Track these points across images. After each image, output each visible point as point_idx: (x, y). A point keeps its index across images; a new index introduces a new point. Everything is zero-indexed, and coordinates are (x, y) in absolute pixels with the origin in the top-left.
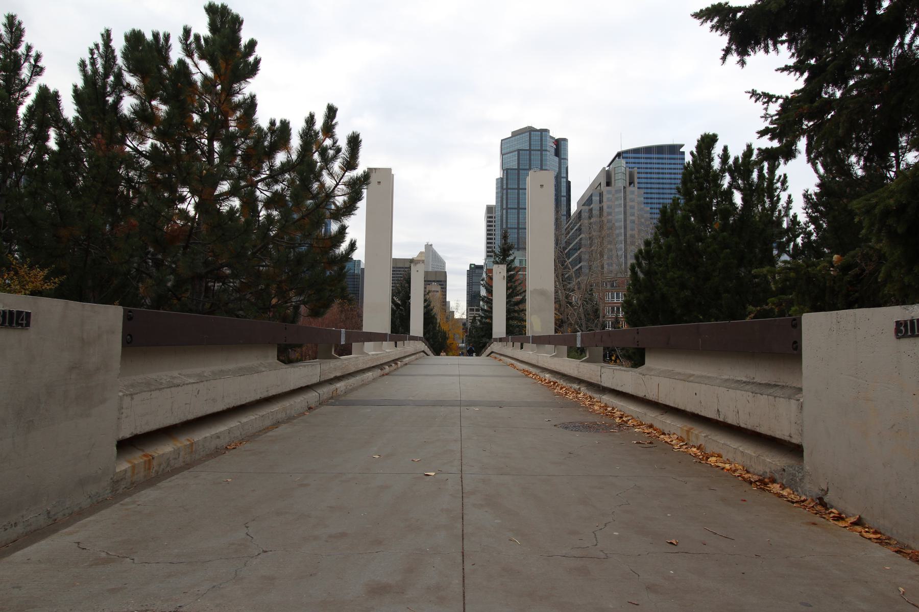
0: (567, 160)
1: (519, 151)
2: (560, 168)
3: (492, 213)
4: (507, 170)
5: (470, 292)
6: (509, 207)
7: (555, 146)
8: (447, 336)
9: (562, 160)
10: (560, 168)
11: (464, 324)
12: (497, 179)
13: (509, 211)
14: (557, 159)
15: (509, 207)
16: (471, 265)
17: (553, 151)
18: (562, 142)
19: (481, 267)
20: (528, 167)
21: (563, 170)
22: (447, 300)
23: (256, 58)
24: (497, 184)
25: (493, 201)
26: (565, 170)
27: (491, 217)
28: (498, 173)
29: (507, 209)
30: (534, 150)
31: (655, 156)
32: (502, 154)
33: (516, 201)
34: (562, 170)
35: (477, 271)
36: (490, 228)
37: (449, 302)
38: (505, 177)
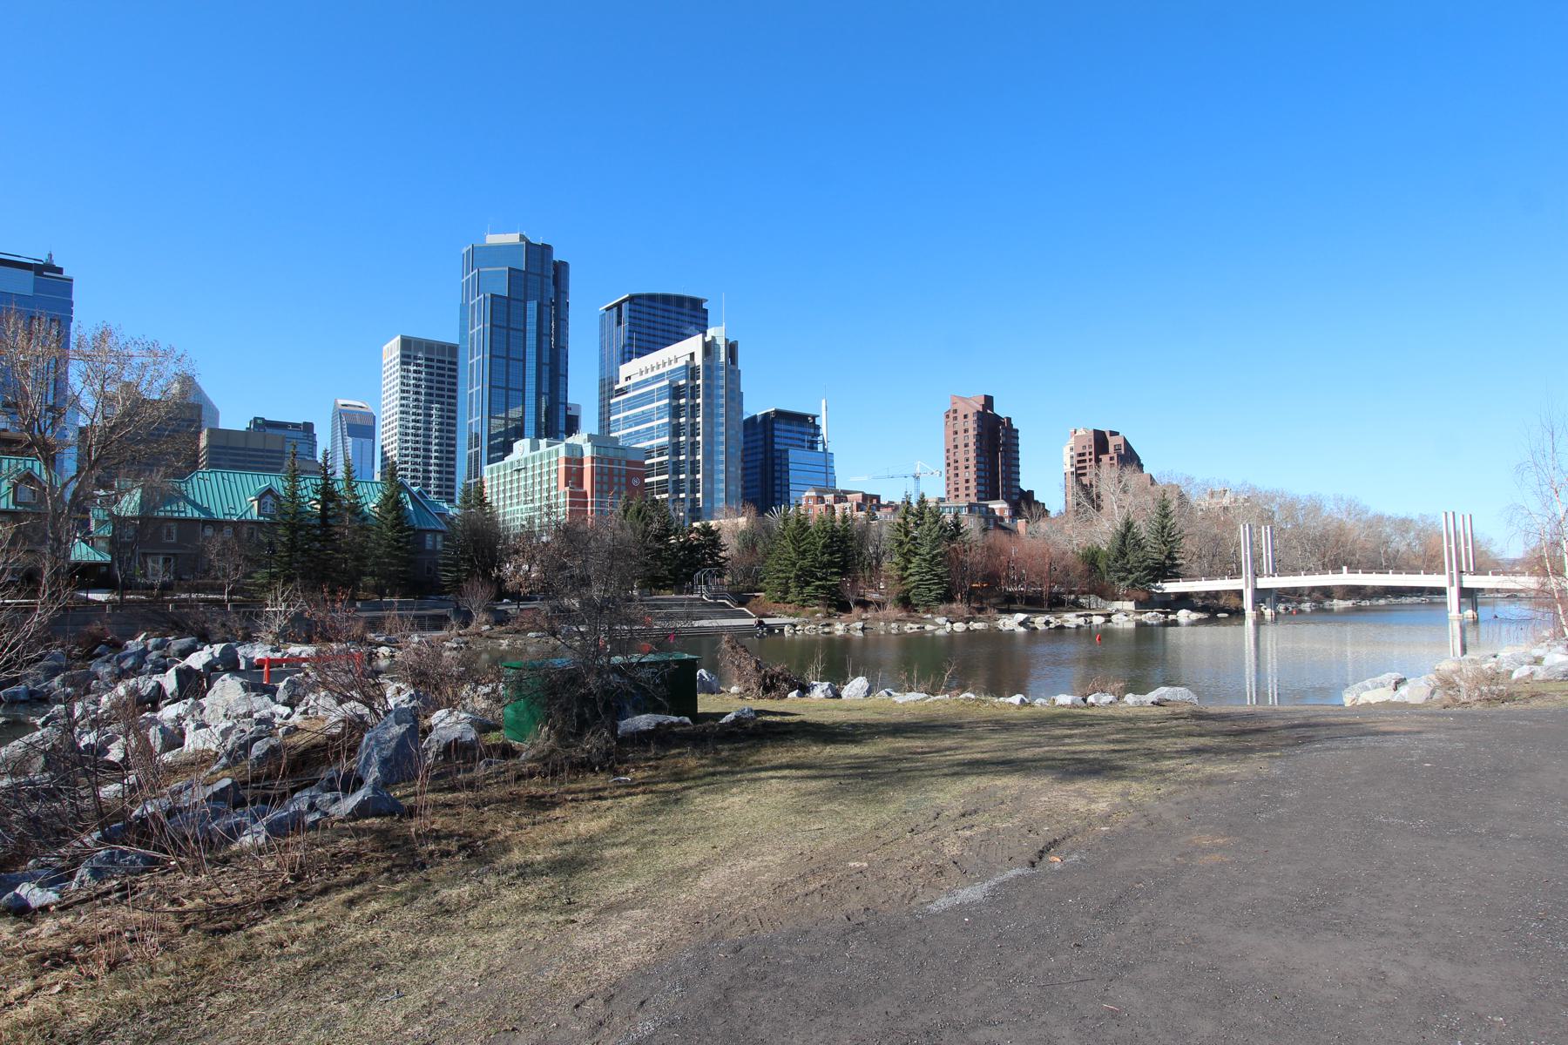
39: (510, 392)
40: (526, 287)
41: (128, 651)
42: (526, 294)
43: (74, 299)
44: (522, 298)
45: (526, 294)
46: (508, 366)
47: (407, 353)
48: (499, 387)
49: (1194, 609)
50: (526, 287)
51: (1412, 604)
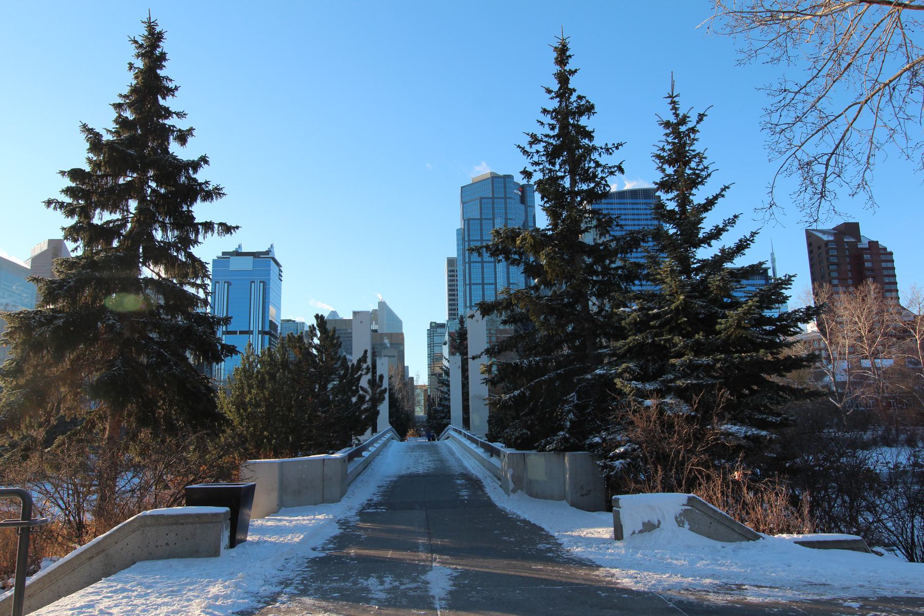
0: (534, 207)
1: (481, 198)
2: (526, 216)
3: (453, 266)
4: (469, 220)
5: (431, 354)
6: (472, 260)
7: (520, 193)
8: (411, 417)
9: (529, 208)
10: (526, 216)
11: (426, 390)
12: (458, 230)
13: (473, 286)
14: (523, 207)
15: (472, 260)
16: (431, 323)
17: (519, 198)
18: (528, 188)
19: (442, 326)
20: (495, 179)
21: (530, 219)
22: (406, 365)
23: (310, 327)
24: (458, 235)
25: (454, 254)
26: (532, 219)
27: (453, 271)
28: (459, 224)
29: (470, 284)
30: (497, 198)
31: (629, 201)
32: (463, 203)
33: (484, 232)
34: (529, 219)
35: (439, 330)
36: (453, 273)
37: (408, 367)
38: (466, 228)
39: (485, 286)
40: (493, 208)
41: (798, 337)
42: (494, 214)
43: (897, 281)
44: (491, 217)
45: (494, 214)
46: (483, 268)
47: (452, 268)
48: (477, 284)
49: (546, 557)
50: (493, 208)
51: (902, 552)
